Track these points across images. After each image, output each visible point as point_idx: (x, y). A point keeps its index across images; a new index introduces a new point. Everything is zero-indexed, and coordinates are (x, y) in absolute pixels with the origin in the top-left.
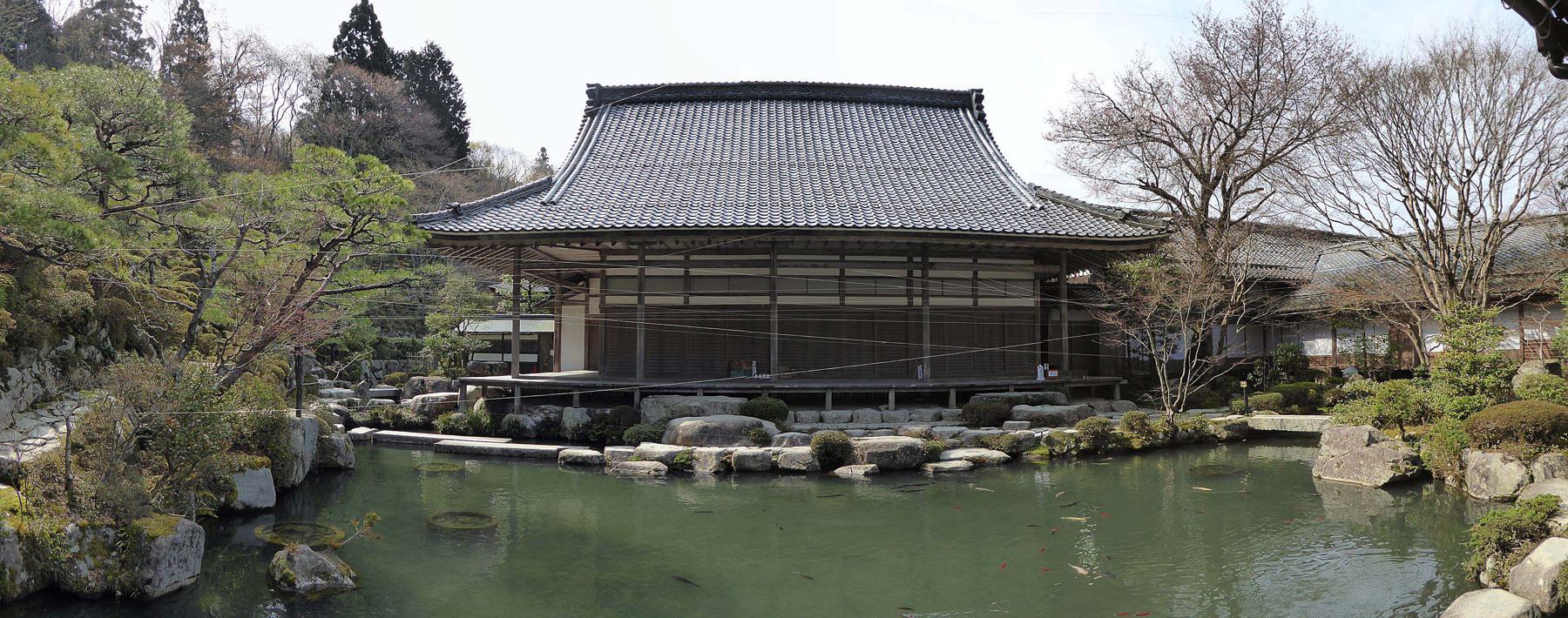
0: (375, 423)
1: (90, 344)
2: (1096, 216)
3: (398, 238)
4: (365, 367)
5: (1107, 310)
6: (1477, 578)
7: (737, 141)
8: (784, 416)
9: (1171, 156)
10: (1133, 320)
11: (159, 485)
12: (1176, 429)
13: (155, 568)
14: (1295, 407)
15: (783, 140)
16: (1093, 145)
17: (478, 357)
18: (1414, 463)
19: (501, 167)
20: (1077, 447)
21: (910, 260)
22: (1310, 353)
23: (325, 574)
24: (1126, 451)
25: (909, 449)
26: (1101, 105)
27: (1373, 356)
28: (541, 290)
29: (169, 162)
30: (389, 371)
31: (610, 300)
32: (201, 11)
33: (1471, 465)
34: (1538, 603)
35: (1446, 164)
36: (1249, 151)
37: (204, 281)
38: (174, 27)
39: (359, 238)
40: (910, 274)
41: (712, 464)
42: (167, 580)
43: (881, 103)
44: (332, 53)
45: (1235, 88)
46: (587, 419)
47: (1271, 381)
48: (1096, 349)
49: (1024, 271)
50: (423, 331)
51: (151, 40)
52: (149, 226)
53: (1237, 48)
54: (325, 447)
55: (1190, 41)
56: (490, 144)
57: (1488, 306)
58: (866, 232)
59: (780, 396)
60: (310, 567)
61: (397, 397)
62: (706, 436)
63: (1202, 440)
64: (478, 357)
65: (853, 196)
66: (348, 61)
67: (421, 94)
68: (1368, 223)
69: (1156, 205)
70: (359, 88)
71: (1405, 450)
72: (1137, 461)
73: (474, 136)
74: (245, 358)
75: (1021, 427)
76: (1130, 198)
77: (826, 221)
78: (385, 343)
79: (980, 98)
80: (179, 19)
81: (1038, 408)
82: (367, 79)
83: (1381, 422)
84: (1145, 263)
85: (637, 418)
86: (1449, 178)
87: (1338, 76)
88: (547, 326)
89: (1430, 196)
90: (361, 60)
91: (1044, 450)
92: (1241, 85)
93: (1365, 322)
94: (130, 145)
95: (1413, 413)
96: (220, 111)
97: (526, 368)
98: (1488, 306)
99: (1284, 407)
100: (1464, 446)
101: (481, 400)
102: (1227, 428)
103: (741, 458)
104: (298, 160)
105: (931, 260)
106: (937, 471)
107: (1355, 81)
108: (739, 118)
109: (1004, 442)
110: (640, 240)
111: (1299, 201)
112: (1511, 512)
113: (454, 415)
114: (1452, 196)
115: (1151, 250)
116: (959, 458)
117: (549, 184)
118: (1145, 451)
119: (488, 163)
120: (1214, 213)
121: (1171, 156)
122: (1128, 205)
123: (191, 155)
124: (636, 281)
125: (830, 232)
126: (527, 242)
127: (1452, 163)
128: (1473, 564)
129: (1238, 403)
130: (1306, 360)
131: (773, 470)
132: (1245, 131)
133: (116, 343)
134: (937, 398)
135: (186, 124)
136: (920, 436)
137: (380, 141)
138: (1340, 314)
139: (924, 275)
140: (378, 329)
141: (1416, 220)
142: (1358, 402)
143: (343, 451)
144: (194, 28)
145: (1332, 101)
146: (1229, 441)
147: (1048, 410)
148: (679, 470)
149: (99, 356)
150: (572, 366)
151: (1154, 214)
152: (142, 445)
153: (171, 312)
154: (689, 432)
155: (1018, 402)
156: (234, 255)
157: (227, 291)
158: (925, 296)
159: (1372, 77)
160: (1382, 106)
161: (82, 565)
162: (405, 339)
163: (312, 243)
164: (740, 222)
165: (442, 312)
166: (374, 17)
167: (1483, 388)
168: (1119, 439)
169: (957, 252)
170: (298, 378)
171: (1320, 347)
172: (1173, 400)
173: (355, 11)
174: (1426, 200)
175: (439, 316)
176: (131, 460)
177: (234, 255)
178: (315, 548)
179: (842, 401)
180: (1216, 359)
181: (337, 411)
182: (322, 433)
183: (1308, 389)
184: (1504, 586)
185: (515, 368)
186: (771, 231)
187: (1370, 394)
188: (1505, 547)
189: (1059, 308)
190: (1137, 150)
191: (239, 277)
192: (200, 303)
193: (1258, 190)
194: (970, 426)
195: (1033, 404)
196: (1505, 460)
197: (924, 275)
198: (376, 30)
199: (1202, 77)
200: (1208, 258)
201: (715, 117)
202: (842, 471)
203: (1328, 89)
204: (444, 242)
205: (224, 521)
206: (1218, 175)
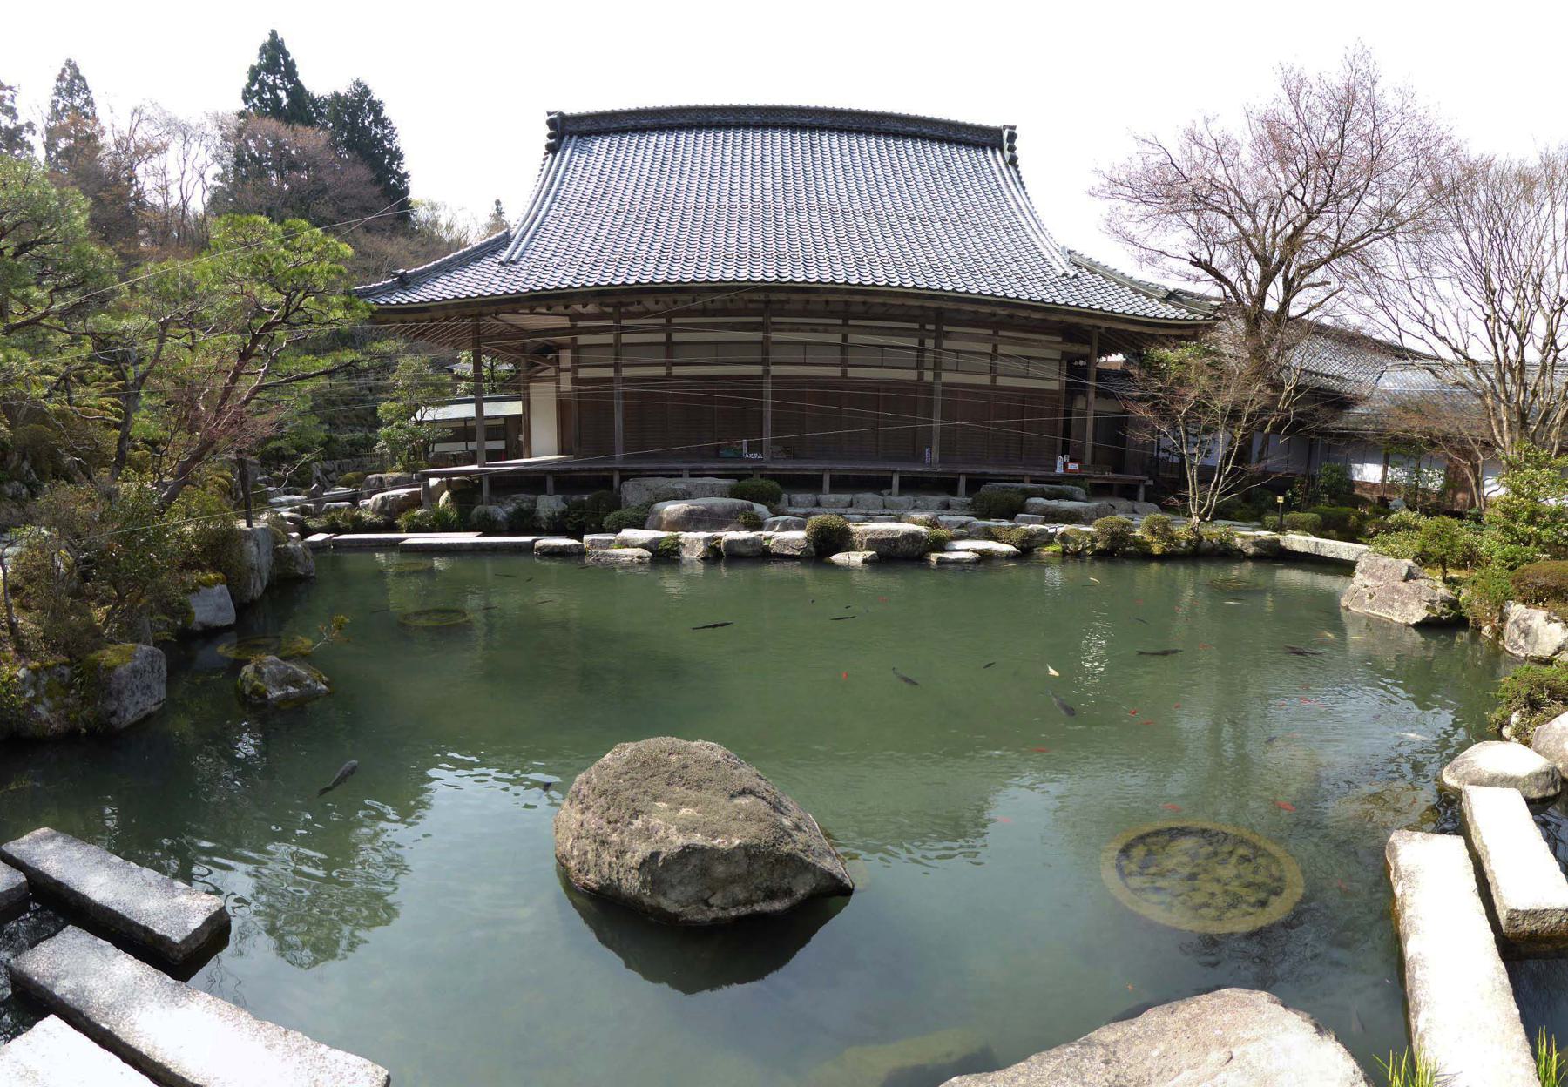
0: (334, 528)
1: (12, 479)
2: (1136, 291)
3: (339, 314)
4: (316, 469)
5: (1141, 399)
6: (1499, 731)
7: (727, 179)
8: (777, 499)
9: (1229, 230)
10: (1165, 413)
11: (109, 614)
12: (1201, 538)
13: (117, 699)
14: (1333, 532)
15: (779, 179)
16: (1142, 207)
17: (439, 448)
18: (1451, 607)
19: (450, 227)
20: (1093, 546)
21: (922, 326)
22: (1357, 478)
23: (296, 681)
24: (1145, 556)
25: (912, 537)
26: (1156, 158)
27: (1425, 490)
28: (505, 368)
29: (70, 259)
30: (343, 472)
31: (584, 373)
32: (82, 79)
33: (1513, 618)
34: (1560, 766)
35: (1539, 286)
36: (1320, 237)
37: (128, 396)
38: (54, 104)
39: (295, 318)
40: (922, 343)
41: (700, 549)
42: (132, 710)
43: (896, 135)
44: (242, 106)
45: (1313, 159)
46: (562, 507)
47: (1311, 502)
48: (1122, 441)
49: (1050, 348)
50: (378, 424)
51: (30, 125)
52: (60, 338)
53: (1321, 109)
54: (282, 557)
55: (1268, 96)
56: (435, 200)
57: (1558, 455)
58: (872, 292)
59: (773, 477)
60: (279, 677)
61: (354, 499)
62: (691, 521)
63: (1226, 554)
64: (439, 448)
65: (859, 248)
66: (262, 114)
67: (350, 145)
68: (1443, 339)
69: (1209, 288)
70: (278, 146)
71: (1443, 591)
72: (1155, 566)
73: (418, 191)
74: (184, 469)
75: (1034, 521)
76: (1176, 275)
77: (827, 278)
78: (335, 441)
79: (1012, 137)
80: (59, 92)
81: (1054, 503)
82: (286, 133)
83: (1423, 559)
84: (1186, 352)
85: (617, 504)
86: (1539, 303)
87: (1433, 162)
88: (515, 408)
89: (1516, 323)
90: (276, 111)
91: (1056, 547)
92: (1321, 156)
93: (1421, 452)
94: (23, 248)
95: (1459, 555)
96: (120, 197)
97: (494, 456)
98: (1558, 455)
99: (1321, 530)
100: (1508, 597)
101: (446, 494)
102: (1255, 544)
103: (731, 543)
104: (216, 235)
105: (946, 328)
106: (941, 561)
107: (1450, 171)
108: (729, 149)
109: (1015, 535)
110: (613, 300)
111: (1367, 302)
112: (1547, 671)
113: (418, 512)
114: (1539, 327)
115: (1194, 338)
116: (965, 549)
117: (505, 241)
118: (1163, 558)
119: (435, 224)
120: (1271, 305)
121: (1229, 230)
122: (1172, 284)
123: (95, 249)
124: (612, 350)
125: (833, 289)
126: (485, 310)
127: (1545, 287)
128: (1497, 715)
129: (1271, 518)
130: (1352, 485)
131: (763, 555)
132: (1319, 211)
133: (41, 474)
134: (946, 485)
135: (83, 212)
136: (924, 524)
137: (307, 202)
138: (1396, 438)
139: (938, 345)
140: (326, 427)
141: (1495, 345)
142: (1401, 535)
143: (301, 559)
144: (78, 102)
145: (1422, 192)
146: (1255, 558)
147: (1066, 505)
148: (665, 556)
149: (24, 491)
150: (544, 449)
151: (1201, 297)
152: (85, 576)
153: (97, 432)
154: (674, 516)
155: (1034, 494)
156: (156, 359)
157: (155, 401)
158: (937, 367)
159: (1471, 173)
160: (1477, 206)
161: (41, 709)
162: (357, 435)
163: (242, 332)
164: (729, 276)
165: (396, 400)
166: (286, 54)
167: (1539, 542)
168: (1138, 543)
169: (976, 321)
170: (244, 489)
171: (1370, 472)
172: (1201, 507)
173: (263, 50)
174: (1510, 323)
175: (392, 405)
176: (76, 594)
177: (156, 359)
178: (284, 659)
179: (842, 484)
180: (1253, 467)
181: (290, 519)
182: (277, 542)
183: (1351, 515)
184: (1527, 743)
185: (482, 457)
186: (765, 288)
187: (1417, 528)
188: (1534, 705)
189: (1085, 394)
190: (1191, 218)
191: (168, 385)
192: (128, 414)
193: (1324, 283)
194: (979, 517)
195: (1049, 498)
196: (1549, 620)
197: (938, 345)
198: (290, 72)
199: (1278, 141)
200: (1258, 353)
201: (700, 148)
202: (839, 558)
203: (1421, 177)
204: (393, 317)
205: (183, 646)
206: (1283, 259)
